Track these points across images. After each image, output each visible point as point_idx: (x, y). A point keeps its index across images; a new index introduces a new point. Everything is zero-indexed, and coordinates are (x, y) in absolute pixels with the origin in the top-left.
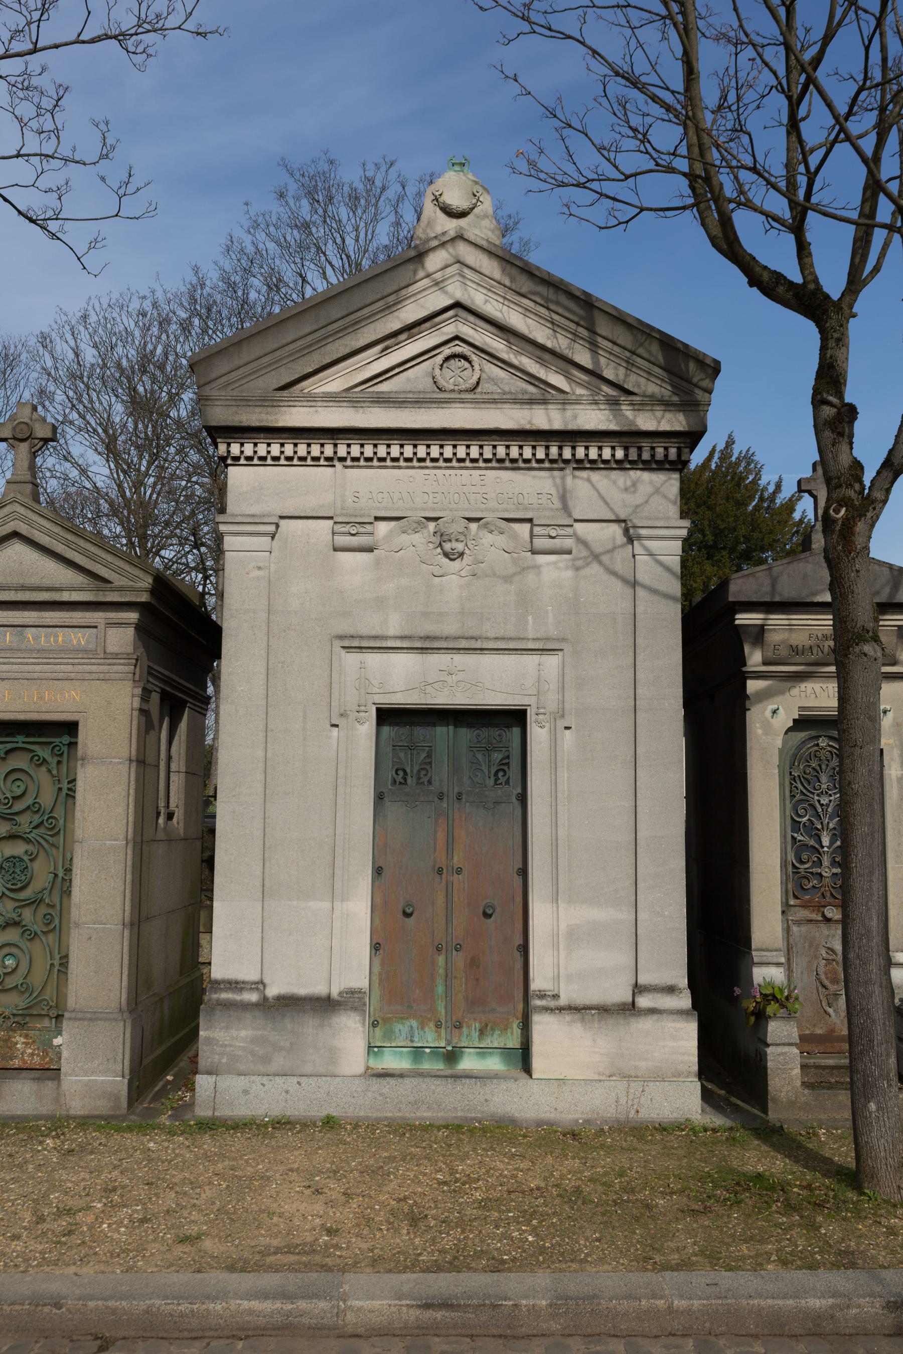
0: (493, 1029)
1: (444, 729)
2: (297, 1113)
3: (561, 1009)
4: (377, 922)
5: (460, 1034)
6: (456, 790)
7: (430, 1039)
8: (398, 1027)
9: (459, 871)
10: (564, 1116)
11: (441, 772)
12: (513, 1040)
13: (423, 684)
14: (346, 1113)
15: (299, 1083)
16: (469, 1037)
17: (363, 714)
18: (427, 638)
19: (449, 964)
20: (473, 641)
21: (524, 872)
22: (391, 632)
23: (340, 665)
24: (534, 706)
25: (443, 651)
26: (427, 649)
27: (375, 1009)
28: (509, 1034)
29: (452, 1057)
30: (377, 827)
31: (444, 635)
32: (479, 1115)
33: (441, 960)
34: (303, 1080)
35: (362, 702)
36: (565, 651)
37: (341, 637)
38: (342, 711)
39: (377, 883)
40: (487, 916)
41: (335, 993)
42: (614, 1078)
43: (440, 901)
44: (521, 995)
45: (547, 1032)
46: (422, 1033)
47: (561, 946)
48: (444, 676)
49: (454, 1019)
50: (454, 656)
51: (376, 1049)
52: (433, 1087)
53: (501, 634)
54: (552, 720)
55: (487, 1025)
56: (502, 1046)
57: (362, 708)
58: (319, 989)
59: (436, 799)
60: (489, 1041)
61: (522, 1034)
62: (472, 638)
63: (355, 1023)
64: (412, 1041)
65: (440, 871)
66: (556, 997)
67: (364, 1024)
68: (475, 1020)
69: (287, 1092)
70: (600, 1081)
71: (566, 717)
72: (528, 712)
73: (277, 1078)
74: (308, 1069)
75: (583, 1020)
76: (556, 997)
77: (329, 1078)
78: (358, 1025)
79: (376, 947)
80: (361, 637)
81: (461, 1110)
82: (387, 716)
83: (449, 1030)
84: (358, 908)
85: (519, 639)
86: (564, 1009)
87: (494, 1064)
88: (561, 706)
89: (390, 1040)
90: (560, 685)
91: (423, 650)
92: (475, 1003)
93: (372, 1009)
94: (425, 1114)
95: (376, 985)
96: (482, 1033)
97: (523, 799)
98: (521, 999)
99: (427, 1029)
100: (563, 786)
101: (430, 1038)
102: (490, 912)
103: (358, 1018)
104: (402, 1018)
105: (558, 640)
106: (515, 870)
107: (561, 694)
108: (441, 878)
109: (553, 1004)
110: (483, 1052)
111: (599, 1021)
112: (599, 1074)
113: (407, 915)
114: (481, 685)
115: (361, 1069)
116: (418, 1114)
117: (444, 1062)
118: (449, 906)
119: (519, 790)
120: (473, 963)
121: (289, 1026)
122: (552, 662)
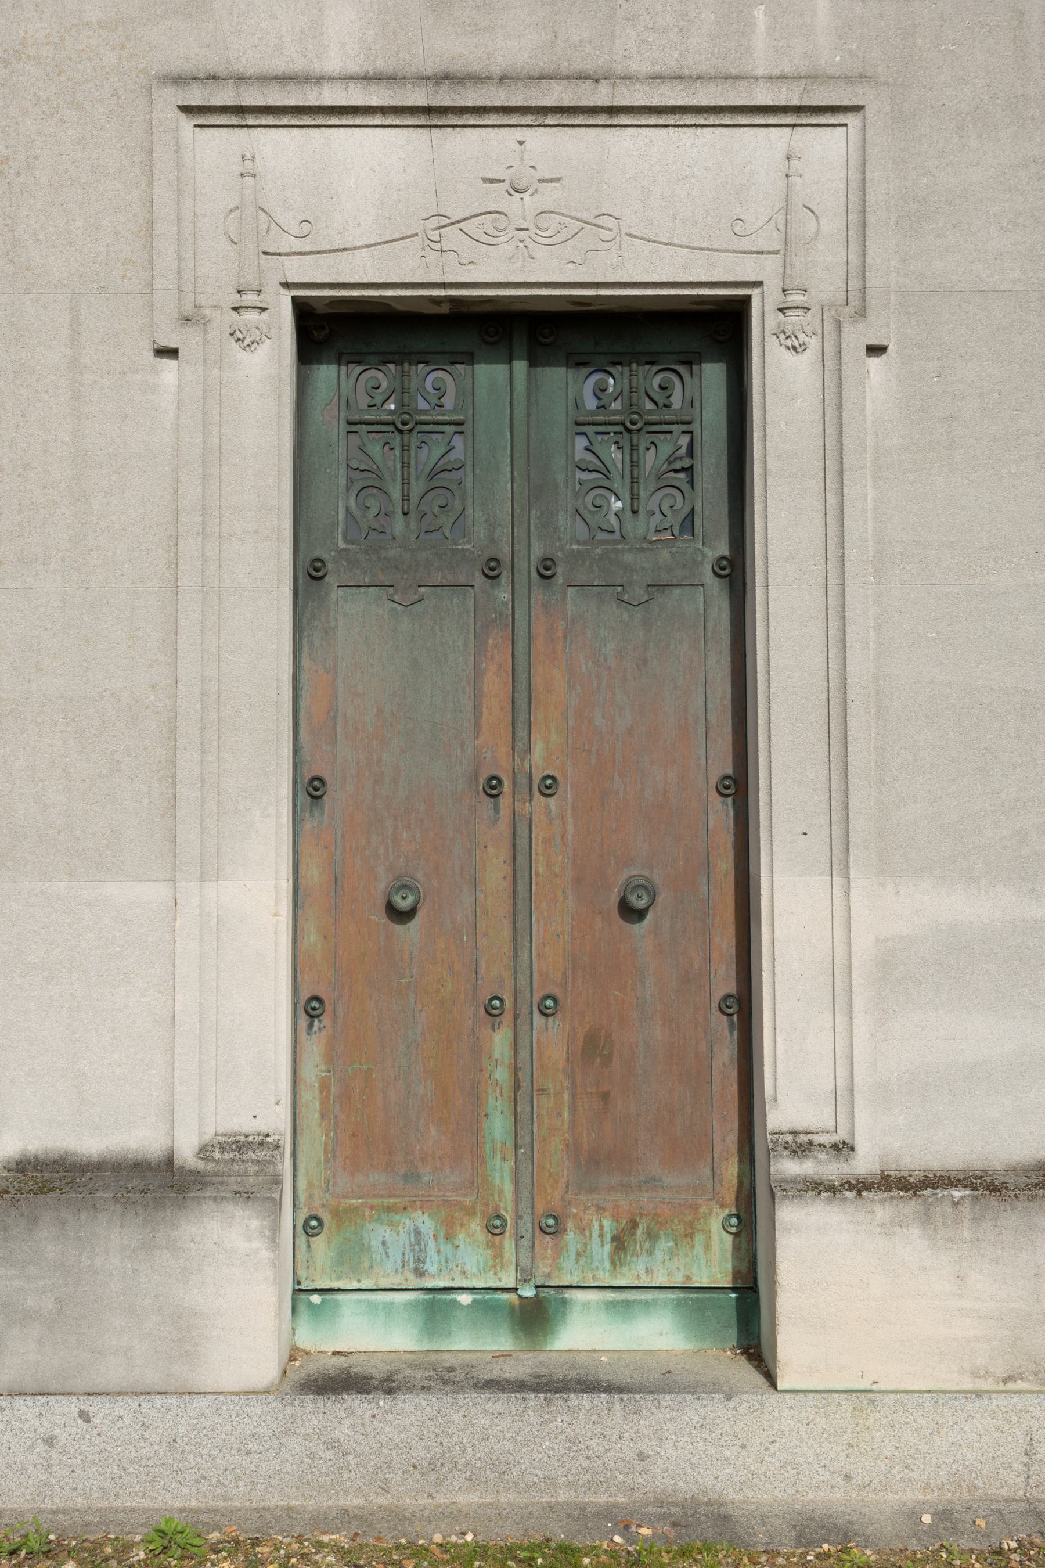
0: (652, 1237)
1: (500, 370)
2: (80, 1502)
3: (860, 1186)
4: (312, 938)
5: (559, 1251)
6: (537, 551)
7: (471, 1268)
8: (377, 1233)
9: (549, 787)
10: (870, 1496)
11: (491, 512)
12: (712, 1263)
13: (435, 222)
14: (226, 1498)
15: (84, 1416)
16: (583, 1256)
17: (251, 317)
18: (445, 78)
19: (524, 1054)
20: (587, 86)
21: (739, 787)
22: (332, 63)
23: (179, 165)
24: (773, 285)
25: (493, 119)
26: (444, 111)
27: (310, 1185)
28: (699, 1249)
29: (535, 1316)
30: (305, 662)
31: (496, 70)
32: (620, 1499)
33: (500, 1042)
34: (97, 1407)
35: (250, 278)
36: (869, 111)
37: (179, 80)
38: (188, 309)
39: (308, 825)
40: (630, 913)
41: (187, 1153)
42: (1020, 1385)
43: (495, 873)
44: (732, 1139)
45: (815, 1250)
46: (447, 1248)
47: (858, 1003)
48: (496, 198)
49: (540, 1208)
50: (532, 136)
51: (316, 1299)
52: (484, 1421)
53: (671, 63)
54: (829, 327)
55: (634, 1225)
56: (678, 1280)
57: (250, 298)
58: (139, 1137)
59: (479, 580)
60: (641, 1269)
61: (736, 1248)
62: (582, 77)
63: (249, 1240)
64: (420, 1273)
65: (493, 788)
66: (843, 1148)
67: (274, 1241)
68: (600, 1209)
69: (50, 1442)
70: (978, 1394)
71: (871, 317)
72: (755, 303)
73: (19, 1401)
74: (111, 1372)
75: (926, 1219)
76: (843, 1148)
77: (173, 1400)
78: (256, 1244)
79: (310, 1009)
80: (241, 79)
81: (569, 1484)
82: (333, 329)
83: (525, 1243)
84: (245, 908)
85: (727, 77)
86: (869, 1187)
87: (657, 1335)
88: (854, 283)
89: (356, 1270)
90: (854, 217)
91: (432, 115)
92: (599, 1162)
93: (302, 1184)
94: (462, 1499)
95: (312, 1115)
96: (620, 1244)
97: (736, 573)
98: (734, 1148)
99: (461, 1238)
100: (861, 528)
101: (470, 1262)
102: (641, 904)
103: (255, 1224)
104: (389, 1209)
105: (848, 79)
106: (714, 780)
107: (854, 248)
108: (497, 809)
109: (833, 1170)
110: (625, 1300)
111: (976, 1220)
112: (975, 1374)
113: (399, 915)
114: (609, 222)
115: (265, 1369)
116: (440, 1499)
117: (513, 1331)
118: (522, 888)
119: (723, 548)
120: (593, 1048)
121: (51, 1251)
122: (826, 147)
